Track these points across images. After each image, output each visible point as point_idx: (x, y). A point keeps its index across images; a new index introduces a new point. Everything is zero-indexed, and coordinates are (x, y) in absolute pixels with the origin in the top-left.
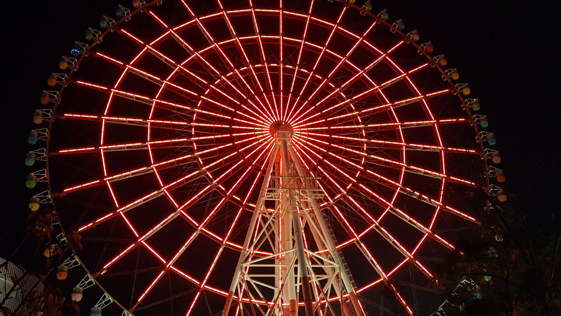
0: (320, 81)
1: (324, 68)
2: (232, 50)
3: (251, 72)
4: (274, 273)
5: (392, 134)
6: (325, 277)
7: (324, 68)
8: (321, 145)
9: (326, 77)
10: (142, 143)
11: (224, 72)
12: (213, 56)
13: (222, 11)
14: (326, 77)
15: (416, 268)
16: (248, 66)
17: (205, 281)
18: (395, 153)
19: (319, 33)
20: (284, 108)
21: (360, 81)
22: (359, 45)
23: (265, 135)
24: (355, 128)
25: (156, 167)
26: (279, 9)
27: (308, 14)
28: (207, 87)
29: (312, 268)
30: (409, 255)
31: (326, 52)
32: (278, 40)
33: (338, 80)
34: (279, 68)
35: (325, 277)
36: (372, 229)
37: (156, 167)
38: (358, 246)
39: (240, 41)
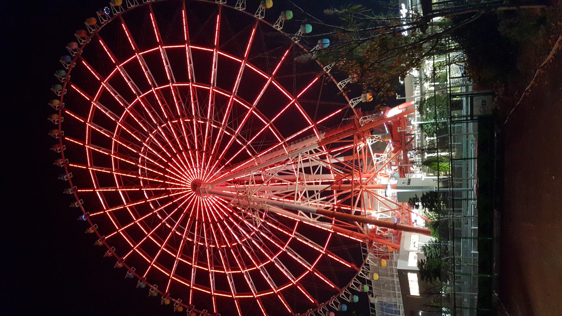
1: (144, 209)
4: (309, 167)
5: (123, 135)
8: (222, 214)
15: (162, 35)
18: (128, 121)
19: (135, 234)
20: (189, 201)
21: (92, 143)
22: (111, 207)
23: (195, 169)
26: (152, 266)
27: (134, 251)
29: (309, 196)
30: (161, 49)
31: (137, 219)
32: (165, 247)
36: (177, 83)
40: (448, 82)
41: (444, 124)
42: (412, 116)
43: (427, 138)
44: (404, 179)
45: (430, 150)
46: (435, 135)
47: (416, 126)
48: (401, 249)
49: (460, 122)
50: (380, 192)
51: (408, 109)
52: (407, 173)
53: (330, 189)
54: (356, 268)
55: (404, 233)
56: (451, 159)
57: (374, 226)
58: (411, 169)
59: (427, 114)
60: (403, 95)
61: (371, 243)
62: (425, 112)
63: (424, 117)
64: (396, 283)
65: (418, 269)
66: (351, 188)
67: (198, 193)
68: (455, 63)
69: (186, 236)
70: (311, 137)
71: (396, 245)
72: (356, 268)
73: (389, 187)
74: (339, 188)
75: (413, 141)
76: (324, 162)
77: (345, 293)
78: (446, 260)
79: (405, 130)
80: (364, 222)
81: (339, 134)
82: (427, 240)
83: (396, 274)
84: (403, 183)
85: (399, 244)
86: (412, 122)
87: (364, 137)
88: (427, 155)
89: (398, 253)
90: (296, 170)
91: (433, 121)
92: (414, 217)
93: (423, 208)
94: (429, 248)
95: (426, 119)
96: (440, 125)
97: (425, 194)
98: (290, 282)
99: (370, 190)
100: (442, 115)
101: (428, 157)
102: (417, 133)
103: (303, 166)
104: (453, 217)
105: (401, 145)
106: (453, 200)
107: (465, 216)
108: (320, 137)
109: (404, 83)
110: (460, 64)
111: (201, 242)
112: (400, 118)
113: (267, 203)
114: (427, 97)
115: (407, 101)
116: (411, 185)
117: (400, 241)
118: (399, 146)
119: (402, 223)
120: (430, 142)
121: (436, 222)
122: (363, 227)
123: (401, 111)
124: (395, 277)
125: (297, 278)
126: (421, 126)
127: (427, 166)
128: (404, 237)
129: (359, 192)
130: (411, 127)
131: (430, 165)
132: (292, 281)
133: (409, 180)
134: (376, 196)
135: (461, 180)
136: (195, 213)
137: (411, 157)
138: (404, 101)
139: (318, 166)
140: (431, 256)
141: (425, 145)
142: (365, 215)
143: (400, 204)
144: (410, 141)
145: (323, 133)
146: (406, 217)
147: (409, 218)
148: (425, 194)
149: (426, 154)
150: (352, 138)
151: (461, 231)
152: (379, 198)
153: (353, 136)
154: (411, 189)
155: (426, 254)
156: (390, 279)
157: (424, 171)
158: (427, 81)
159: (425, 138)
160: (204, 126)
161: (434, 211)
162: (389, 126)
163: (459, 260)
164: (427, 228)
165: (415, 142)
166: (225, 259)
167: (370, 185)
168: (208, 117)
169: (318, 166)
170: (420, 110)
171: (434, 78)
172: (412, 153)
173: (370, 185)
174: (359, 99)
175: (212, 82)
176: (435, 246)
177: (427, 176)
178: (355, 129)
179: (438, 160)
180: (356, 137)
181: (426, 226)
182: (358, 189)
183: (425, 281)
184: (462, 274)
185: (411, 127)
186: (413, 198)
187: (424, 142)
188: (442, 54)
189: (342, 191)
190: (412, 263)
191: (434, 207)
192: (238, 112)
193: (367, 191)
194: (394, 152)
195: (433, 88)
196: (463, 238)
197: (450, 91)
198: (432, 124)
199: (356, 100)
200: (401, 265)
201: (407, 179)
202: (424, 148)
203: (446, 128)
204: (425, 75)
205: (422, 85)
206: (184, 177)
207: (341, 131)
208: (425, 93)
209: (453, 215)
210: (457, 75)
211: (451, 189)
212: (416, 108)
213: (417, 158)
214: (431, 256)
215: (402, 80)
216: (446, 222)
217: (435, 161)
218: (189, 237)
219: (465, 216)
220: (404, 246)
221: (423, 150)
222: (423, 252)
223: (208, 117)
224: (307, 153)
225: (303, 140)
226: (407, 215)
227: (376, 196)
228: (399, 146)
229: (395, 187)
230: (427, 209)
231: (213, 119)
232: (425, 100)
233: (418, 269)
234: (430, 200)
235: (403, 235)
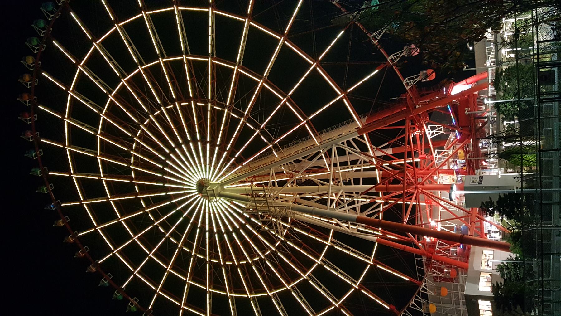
0: (152, 212)
1: (133, 206)
2: (198, 275)
3: (196, 247)
6: (334, 150)
7: (133, 206)
8: (231, 224)
9: (136, 198)
10: (323, 266)
11: (218, 266)
12: (217, 283)
13: (183, 309)
14: (136, 198)
16: (195, 256)
17: (311, 68)
22: (103, 224)
24: (143, 142)
25: (327, 240)
28: (241, 266)
33: (128, 189)
34: (171, 235)
35: (334, 150)
37: (327, 240)
38: (215, 52)
39: (186, 277)
40: (535, 47)
41: (528, 102)
42: (484, 93)
43: (505, 123)
44: (474, 176)
45: (508, 139)
46: (516, 117)
47: (490, 106)
48: (469, 270)
49: (550, 100)
50: (442, 195)
51: (480, 83)
52: (477, 168)
53: (374, 190)
54: (395, 311)
55: (474, 249)
56: (539, 151)
57: (433, 239)
58: (484, 163)
59: (505, 91)
60: (472, 63)
61: (429, 259)
62: (502, 88)
63: (501, 94)
64: (462, 312)
65: (492, 295)
66: (403, 189)
67: (206, 197)
68: (545, 22)
69: (196, 252)
70: (348, 123)
71: (464, 264)
72: (395, 311)
73: (455, 187)
74: (387, 189)
75: (486, 125)
76: (366, 155)
77: (415, 301)
78: (531, 284)
79: (476, 112)
80: (420, 233)
81: (386, 120)
82: (504, 256)
83: (462, 301)
84: (473, 182)
85: (467, 262)
86: (486, 101)
87: (419, 122)
88: (504, 145)
89: (466, 274)
90: (330, 165)
91: (513, 99)
92: (487, 227)
93: (499, 215)
94: (508, 268)
95: (504, 97)
96: (523, 104)
97: (502, 196)
98: (331, 305)
99: (427, 191)
100: (525, 91)
101: (506, 147)
102: (490, 114)
103: (339, 160)
104: (541, 226)
105: (470, 131)
106: (541, 203)
107: (557, 226)
108: (361, 123)
109: (473, 50)
110: (551, 23)
111: (215, 259)
112: (468, 96)
113: (293, 209)
114: (504, 68)
115: (477, 72)
116: (484, 184)
117: (468, 259)
118: (466, 133)
119: (471, 235)
120: (508, 127)
121: (517, 233)
122: (418, 239)
123: (468, 87)
124: (461, 304)
125: (339, 299)
126: (497, 106)
127: (505, 159)
128: (474, 253)
129: (412, 194)
130: (484, 108)
131: (508, 157)
132: (334, 303)
133: (481, 178)
134: (436, 200)
135: (551, 178)
136: (204, 222)
137: (483, 148)
138: (473, 73)
139: (358, 160)
140: (510, 278)
141: (502, 131)
142: (422, 225)
143: (468, 209)
144: (482, 126)
145: (364, 117)
146: (476, 227)
147: (481, 228)
148: (502, 196)
149: (504, 143)
150: (403, 123)
151: (550, 245)
152: (442, 203)
153: (404, 121)
154: (484, 190)
155: (503, 275)
156: (454, 307)
157: (501, 166)
158: (504, 46)
159: (503, 122)
160: (221, 113)
161: (515, 218)
162: (454, 107)
163: (549, 283)
164: (504, 241)
165: (488, 127)
166: (246, 279)
167: (427, 185)
168: (228, 104)
169: (358, 160)
170: (496, 83)
171: (515, 42)
172: (484, 143)
173: (427, 185)
174: (416, 77)
175: (238, 61)
176: (515, 265)
177: (505, 172)
178: (408, 111)
179: (522, 150)
180: (408, 122)
181: (503, 238)
182: (411, 190)
183: (501, 310)
184: (553, 302)
185: (484, 108)
186: (487, 202)
187: (501, 127)
188: (527, 11)
189: (390, 193)
190: (485, 286)
191: (514, 213)
192: (246, 87)
193: (424, 193)
194: (461, 141)
195: (512, 56)
196: (553, 254)
197: (538, 58)
198: (512, 103)
199: (413, 78)
200: (469, 290)
201: (476, 177)
202: (501, 135)
203: (531, 108)
204: (502, 38)
205: (497, 51)
206: (187, 177)
207: (390, 114)
208: (502, 62)
209: (541, 224)
210: (548, 38)
211: (540, 190)
212: (490, 81)
213: (492, 149)
214: (510, 278)
215: (470, 46)
216: (531, 234)
217: (517, 153)
218: (200, 254)
219: (557, 226)
220: (474, 265)
221: (499, 138)
222: (499, 273)
223: (228, 104)
224: (343, 143)
225: (338, 127)
226: (478, 224)
227: (436, 200)
228: (466, 133)
229: (461, 187)
230: (504, 216)
231: (233, 105)
232: (502, 72)
233: (492, 295)
234: (506, 204)
235: (472, 250)
